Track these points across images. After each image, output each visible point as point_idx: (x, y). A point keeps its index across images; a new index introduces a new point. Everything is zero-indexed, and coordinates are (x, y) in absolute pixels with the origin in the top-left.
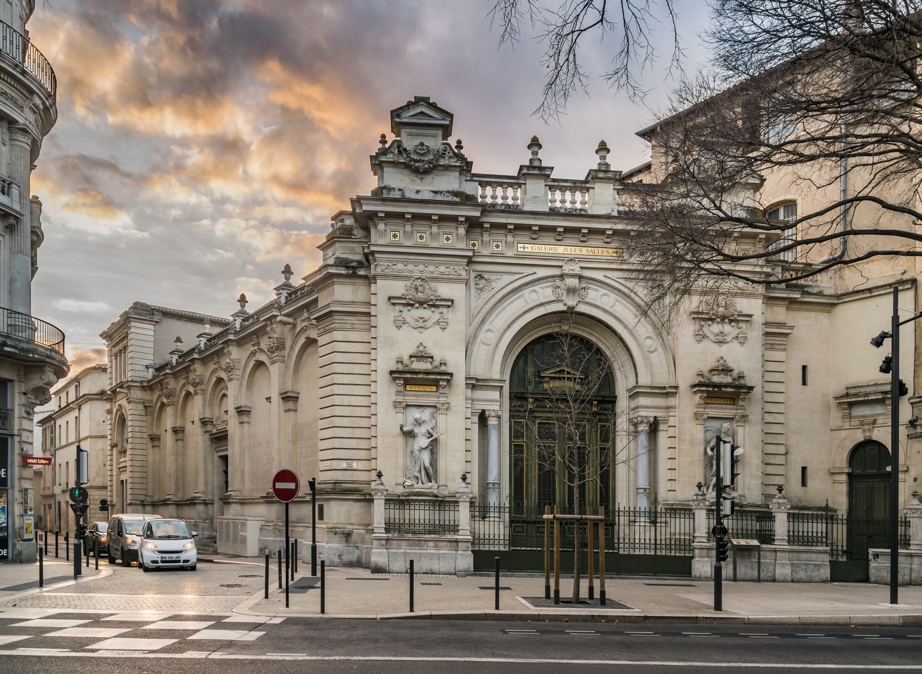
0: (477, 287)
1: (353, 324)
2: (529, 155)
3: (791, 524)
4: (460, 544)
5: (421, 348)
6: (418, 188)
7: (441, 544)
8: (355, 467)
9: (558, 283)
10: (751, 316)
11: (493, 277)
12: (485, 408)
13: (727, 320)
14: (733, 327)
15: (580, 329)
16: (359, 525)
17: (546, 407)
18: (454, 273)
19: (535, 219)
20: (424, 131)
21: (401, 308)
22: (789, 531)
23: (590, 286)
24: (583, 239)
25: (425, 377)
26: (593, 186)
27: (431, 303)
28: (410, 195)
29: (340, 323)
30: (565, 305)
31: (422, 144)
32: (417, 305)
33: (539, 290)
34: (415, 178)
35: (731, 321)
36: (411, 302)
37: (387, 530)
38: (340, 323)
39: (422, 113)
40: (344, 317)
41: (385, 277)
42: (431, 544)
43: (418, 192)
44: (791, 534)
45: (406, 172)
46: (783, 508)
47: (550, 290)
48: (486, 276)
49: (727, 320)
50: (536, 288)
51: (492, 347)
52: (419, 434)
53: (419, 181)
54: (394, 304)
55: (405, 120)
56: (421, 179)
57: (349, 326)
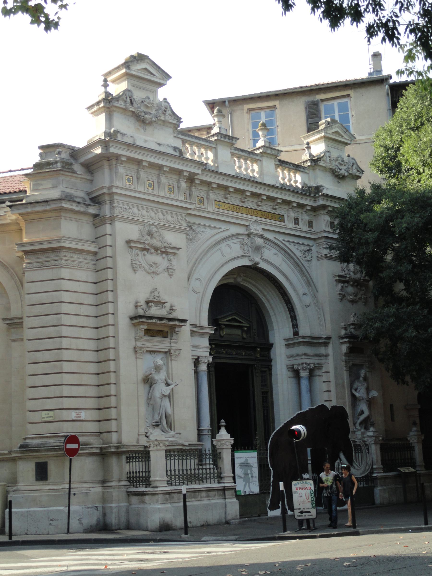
0: (188, 237)
1: (79, 262)
2: (103, 89)
3: (168, 462)
4: (227, 492)
5: (156, 294)
6: (146, 138)
7: (211, 493)
8: (83, 418)
9: (246, 240)
10: (178, 249)
11: (199, 229)
12: (199, 354)
13: (159, 252)
14: (163, 258)
15: (250, 283)
16: (93, 482)
17: (223, 353)
18: (178, 223)
19: (233, 182)
20: (145, 86)
21: (137, 251)
22: (167, 471)
23: (267, 246)
24: (275, 207)
25: (167, 322)
26: (260, 159)
27: (163, 250)
28: (139, 143)
29: (68, 260)
30: (251, 260)
31: (148, 98)
32: (153, 251)
33: (232, 245)
34: (139, 127)
35: (163, 252)
36: (148, 247)
37: (170, 483)
38: (68, 260)
39: (146, 69)
40: (71, 255)
41: (124, 220)
42: (204, 494)
43: (146, 141)
44: (169, 473)
45: (132, 120)
46: (161, 445)
47: (238, 246)
48: (194, 227)
49: (159, 252)
50: (229, 243)
51: (200, 295)
52: (160, 381)
53: (142, 130)
54: (131, 247)
55: (134, 73)
56: (144, 129)
57: (75, 264)
